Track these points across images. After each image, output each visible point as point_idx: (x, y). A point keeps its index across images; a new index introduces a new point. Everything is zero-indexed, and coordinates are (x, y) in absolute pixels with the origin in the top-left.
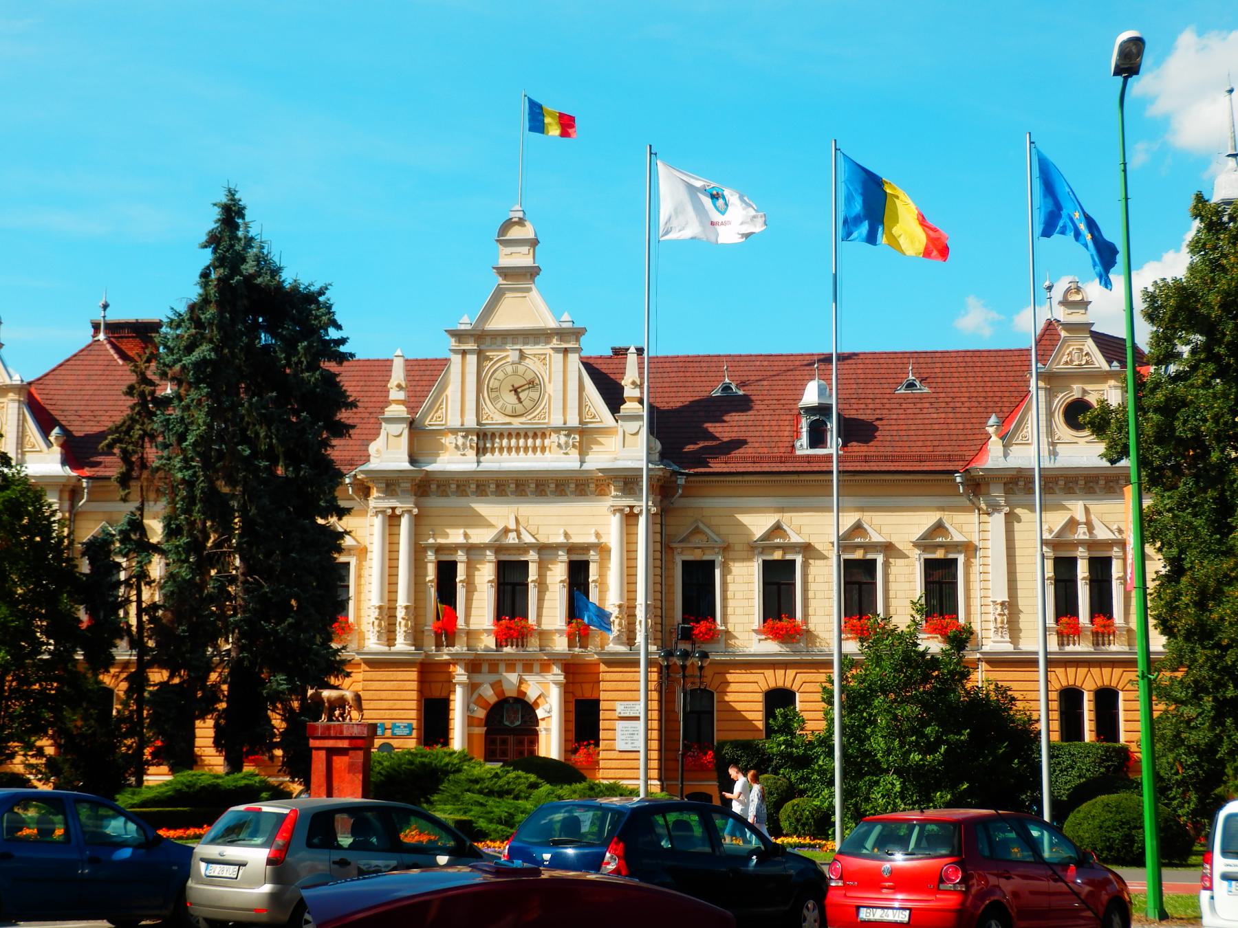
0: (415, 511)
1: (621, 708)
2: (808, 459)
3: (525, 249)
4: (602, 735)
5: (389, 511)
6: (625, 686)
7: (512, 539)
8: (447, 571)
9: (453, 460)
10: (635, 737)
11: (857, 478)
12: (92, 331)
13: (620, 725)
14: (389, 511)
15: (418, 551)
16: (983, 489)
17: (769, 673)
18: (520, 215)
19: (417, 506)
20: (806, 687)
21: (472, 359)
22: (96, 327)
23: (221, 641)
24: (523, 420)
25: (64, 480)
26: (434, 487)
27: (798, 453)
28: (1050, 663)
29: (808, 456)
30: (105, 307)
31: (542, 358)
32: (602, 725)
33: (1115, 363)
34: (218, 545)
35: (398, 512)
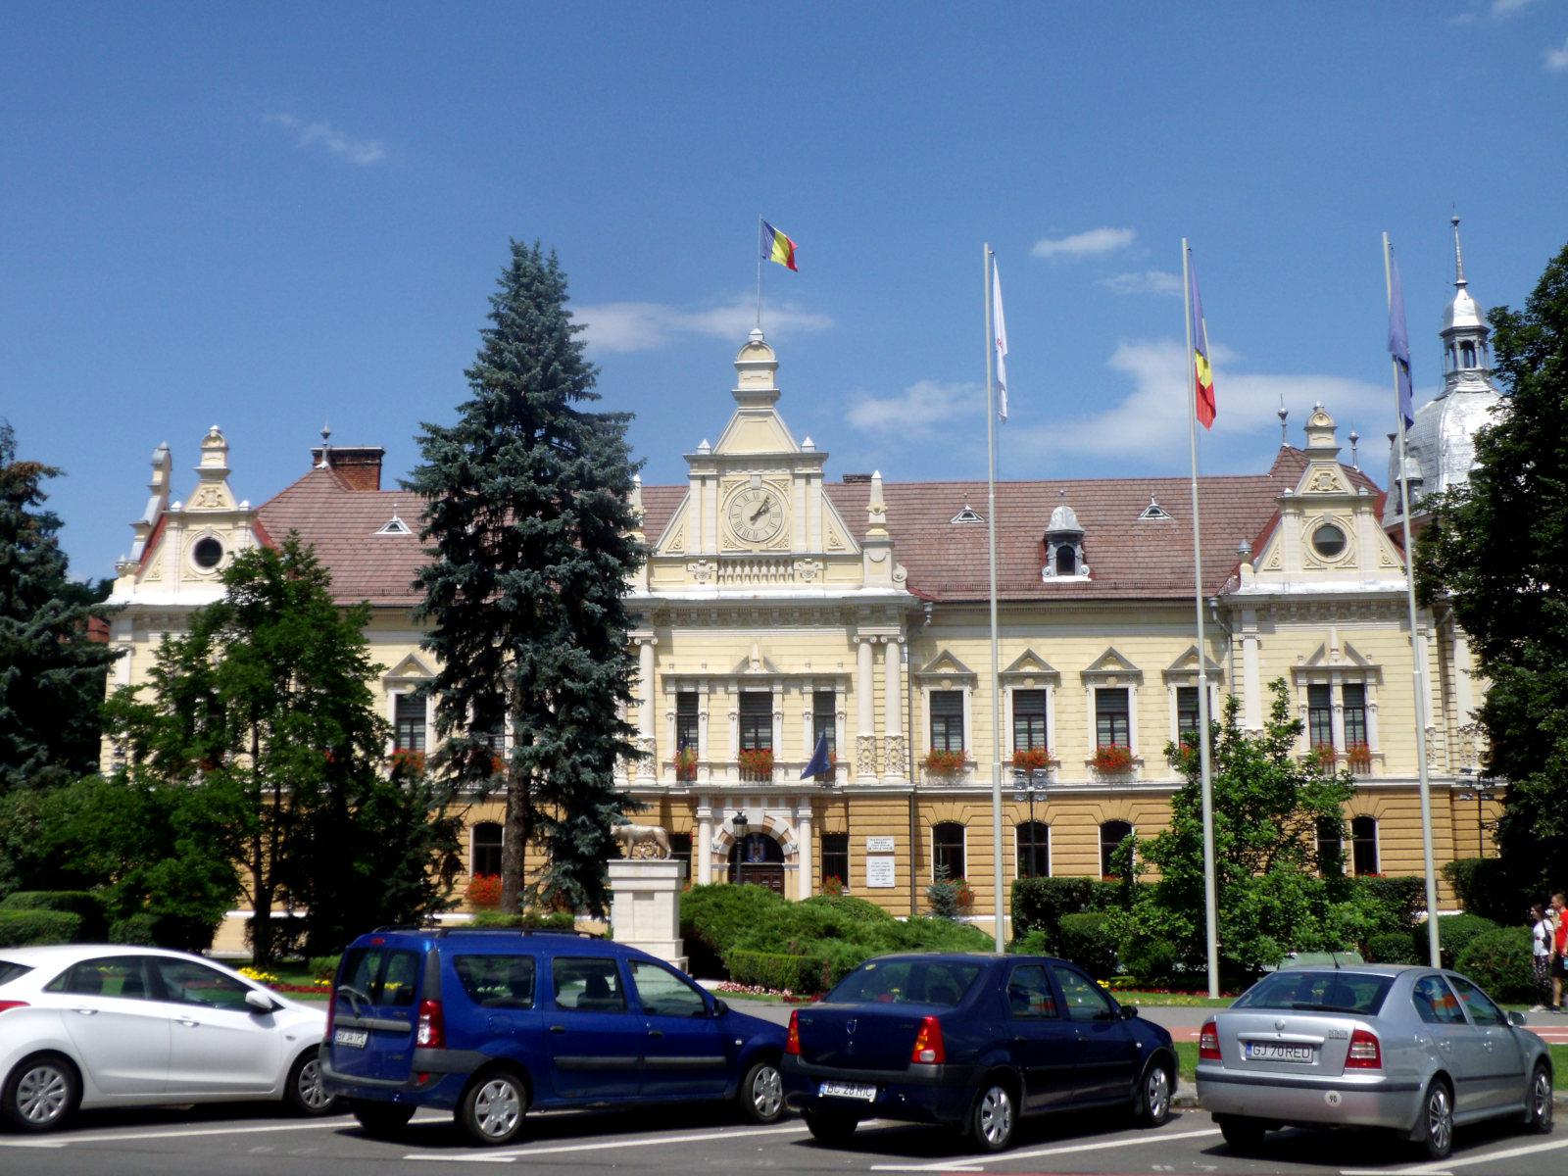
0: (655, 641)
1: (871, 844)
2: (1058, 587)
3: (766, 373)
4: (851, 870)
5: (875, 639)
6: (1409, 813)
7: (756, 669)
10: (887, 873)
11: (1106, 605)
12: (312, 458)
13: (871, 860)
14: (875, 639)
16: (1235, 616)
17: (1104, 803)
18: (760, 338)
19: (656, 635)
20: (1059, 820)
22: (318, 455)
23: (625, 776)
24: (763, 546)
25: (193, 610)
26: (673, 616)
27: (1046, 580)
28: (1006, 797)
29: (1057, 584)
32: (850, 860)
33: (1362, 489)
34: (1561, 669)
35: (883, 640)
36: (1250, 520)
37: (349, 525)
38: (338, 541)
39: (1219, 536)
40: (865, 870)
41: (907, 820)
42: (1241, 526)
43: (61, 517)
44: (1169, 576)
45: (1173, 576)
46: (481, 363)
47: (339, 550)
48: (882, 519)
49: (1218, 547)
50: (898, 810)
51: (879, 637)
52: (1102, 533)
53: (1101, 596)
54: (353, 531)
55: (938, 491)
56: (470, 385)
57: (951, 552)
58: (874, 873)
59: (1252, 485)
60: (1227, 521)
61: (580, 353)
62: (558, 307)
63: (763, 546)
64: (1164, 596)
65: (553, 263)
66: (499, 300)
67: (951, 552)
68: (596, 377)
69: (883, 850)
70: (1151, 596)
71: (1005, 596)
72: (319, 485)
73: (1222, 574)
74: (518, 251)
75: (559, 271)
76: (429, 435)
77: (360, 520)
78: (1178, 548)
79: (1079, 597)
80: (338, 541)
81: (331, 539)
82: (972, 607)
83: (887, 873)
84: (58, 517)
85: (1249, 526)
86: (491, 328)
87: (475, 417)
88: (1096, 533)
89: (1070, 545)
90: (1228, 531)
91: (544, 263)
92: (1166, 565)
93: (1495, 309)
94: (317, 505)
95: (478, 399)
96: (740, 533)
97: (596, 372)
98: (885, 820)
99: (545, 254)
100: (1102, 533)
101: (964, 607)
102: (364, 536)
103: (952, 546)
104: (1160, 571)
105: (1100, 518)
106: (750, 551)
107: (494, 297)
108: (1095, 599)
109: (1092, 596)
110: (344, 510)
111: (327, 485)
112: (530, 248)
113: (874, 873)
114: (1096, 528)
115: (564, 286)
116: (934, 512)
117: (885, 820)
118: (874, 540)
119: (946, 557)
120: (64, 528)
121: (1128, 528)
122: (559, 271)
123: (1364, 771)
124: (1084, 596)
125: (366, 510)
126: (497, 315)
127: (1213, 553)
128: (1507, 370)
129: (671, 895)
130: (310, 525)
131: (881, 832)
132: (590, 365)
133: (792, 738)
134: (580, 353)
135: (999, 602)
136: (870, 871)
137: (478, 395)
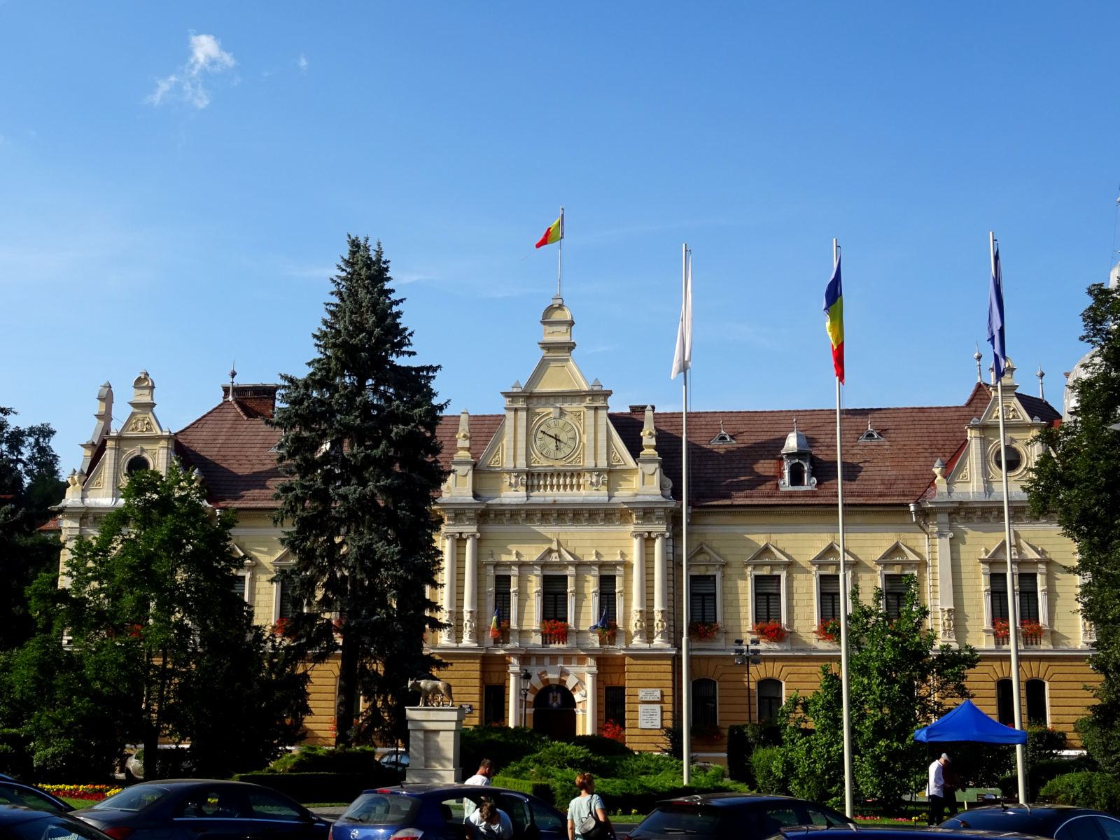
1: (642, 694)
2: (791, 495)
7: (554, 558)
8: (502, 582)
9: (511, 495)
10: (654, 717)
13: (641, 708)
15: (479, 567)
21: (522, 415)
22: (226, 390)
24: (563, 463)
30: (234, 374)
31: (577, 415)
36: (948, 442)
37: (249, 446)
38: (240, 458)
39: (921, 455)
40: (637, 715)
41: (670, 676)
42: (940, 446)
43: (52, 427)
44: (879, 487)
45: (882, 486)
46: (324, 328)
47: (241, 465)
48: (653, 442)
49: (920, 463)
50: (662, 668)
51: (461, 534)
52: (828, 452)
53: (824, 502)
54: (250, 450)
55: (701, 419)
56: (316, 345)
57: (708, 467)
58: (645, 717)
59: (951, 414)
60: (929, 443)
61: (398, 321)
62: (382, 287)
63: (563, 463)
64: (874, 502)
65: (379, 253)
66: (339, 281)
67: (708, 467)
68: (410, 338)
69: (651, 699)
70: (864, 502)
71: (850, 501)
72: (225, 415)
73: (922, 485)
74: (355, 245)
75: (383, 259)
76: (286, 384)
77: (256, 441)
78: (888, 464)
79: (807, 502)
80: (240, 458)
81: (235, 456)
82: (749, 510)
83: (654, 717)
84: (51, 427)
85: (946, 447)
86: (334, 302)
87: (320, 370)
88: (825, 452)
89: (801, 462)
90: (930, 450)
91: (373, 255)
92: (877, 478)
93: (1094, 285)
94: (225, 430)
95: (321, 356)
96: (544, 453)
97: (411, 334)
98: (653, 676)
99: (373, 247)
100: (828, 452)
101: (711, 510)
102: (259, 454)
103: (710, 462)
104: (873, 482)
105: (827, 440)
106: (552, 466)
107: (335, 279)
108: (824, 504)
109: (817, 502)
110: (245, 434)
111: (233, 414)
112: (362, 241)
113: (645, 717)
114: (824, 448)
115: (386, 269)
116: (697, 435)
117: (653, 676)
118: (646, 457)
119: (705, 471)
120: (56, 435)
121: (849, 448)
122: (383, 259)
123: (1037, 644)
124: (810, 502)
125: (261, 434)
126: (339, 294)
127: (916, 468)
128: (1095, 336)
129: (454, 723)
130: (218, 445)
131: (650, 685)
132: (406, 329)
133: (584, 613)
134: (398, 321)
135: (844, 505)
136: (641, 716)
137: (321, 353)
